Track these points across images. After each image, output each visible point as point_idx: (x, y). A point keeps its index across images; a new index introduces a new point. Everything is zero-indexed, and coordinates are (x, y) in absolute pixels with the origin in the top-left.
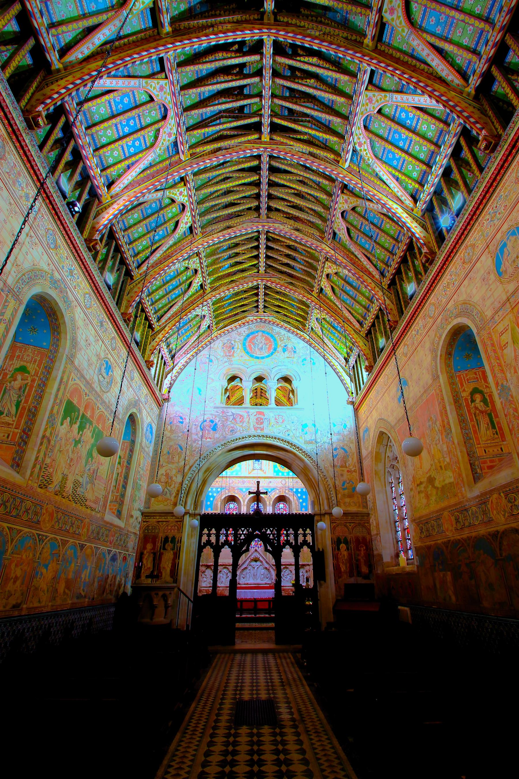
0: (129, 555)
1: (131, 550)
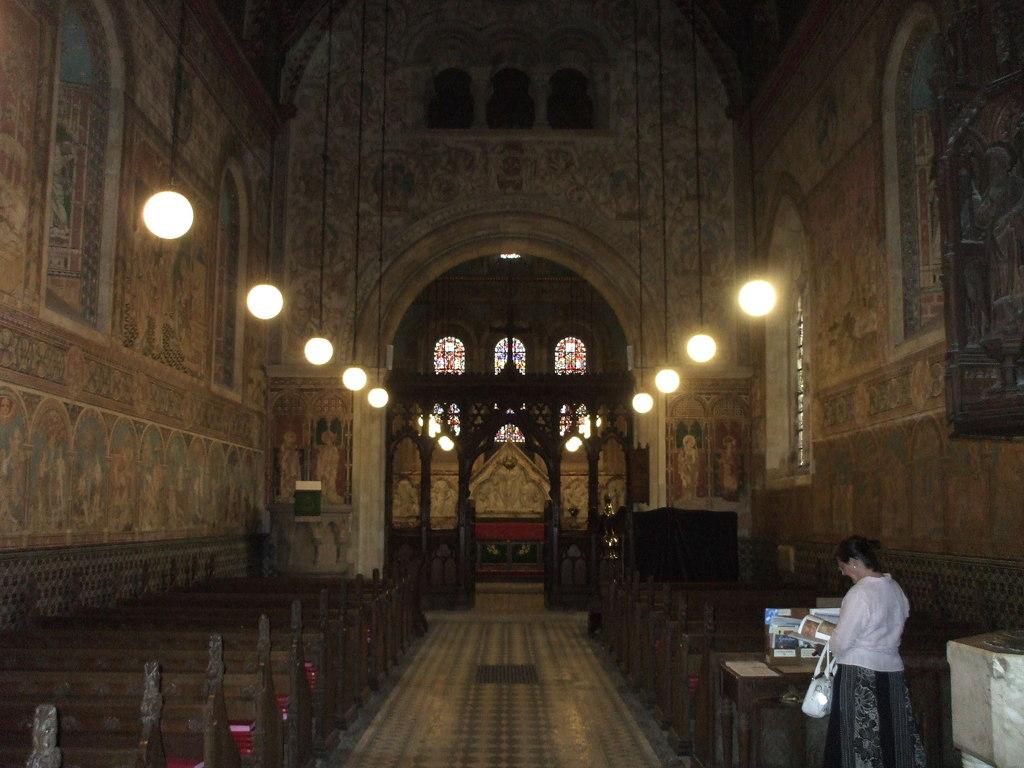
1: (256, 443)
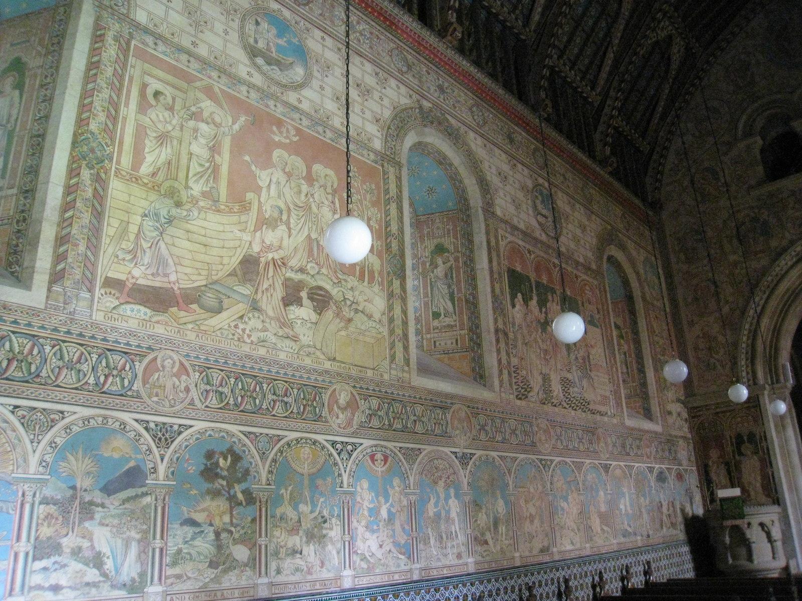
0: (686, 470)
